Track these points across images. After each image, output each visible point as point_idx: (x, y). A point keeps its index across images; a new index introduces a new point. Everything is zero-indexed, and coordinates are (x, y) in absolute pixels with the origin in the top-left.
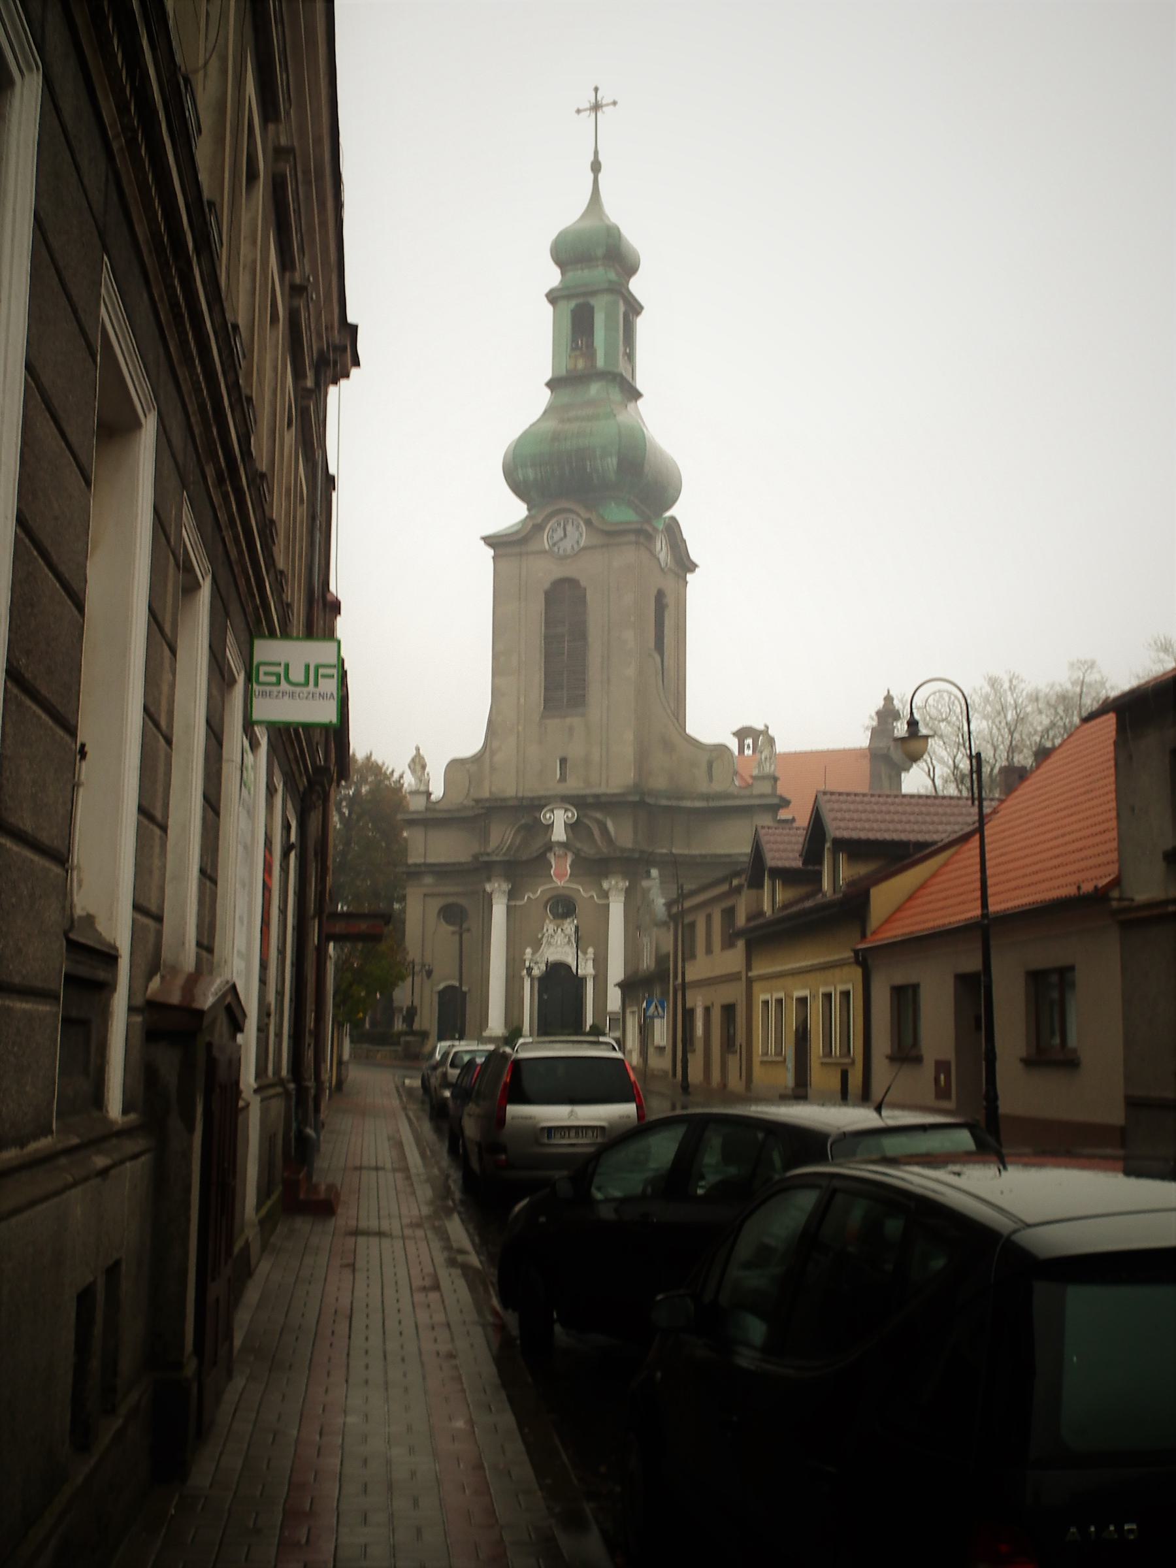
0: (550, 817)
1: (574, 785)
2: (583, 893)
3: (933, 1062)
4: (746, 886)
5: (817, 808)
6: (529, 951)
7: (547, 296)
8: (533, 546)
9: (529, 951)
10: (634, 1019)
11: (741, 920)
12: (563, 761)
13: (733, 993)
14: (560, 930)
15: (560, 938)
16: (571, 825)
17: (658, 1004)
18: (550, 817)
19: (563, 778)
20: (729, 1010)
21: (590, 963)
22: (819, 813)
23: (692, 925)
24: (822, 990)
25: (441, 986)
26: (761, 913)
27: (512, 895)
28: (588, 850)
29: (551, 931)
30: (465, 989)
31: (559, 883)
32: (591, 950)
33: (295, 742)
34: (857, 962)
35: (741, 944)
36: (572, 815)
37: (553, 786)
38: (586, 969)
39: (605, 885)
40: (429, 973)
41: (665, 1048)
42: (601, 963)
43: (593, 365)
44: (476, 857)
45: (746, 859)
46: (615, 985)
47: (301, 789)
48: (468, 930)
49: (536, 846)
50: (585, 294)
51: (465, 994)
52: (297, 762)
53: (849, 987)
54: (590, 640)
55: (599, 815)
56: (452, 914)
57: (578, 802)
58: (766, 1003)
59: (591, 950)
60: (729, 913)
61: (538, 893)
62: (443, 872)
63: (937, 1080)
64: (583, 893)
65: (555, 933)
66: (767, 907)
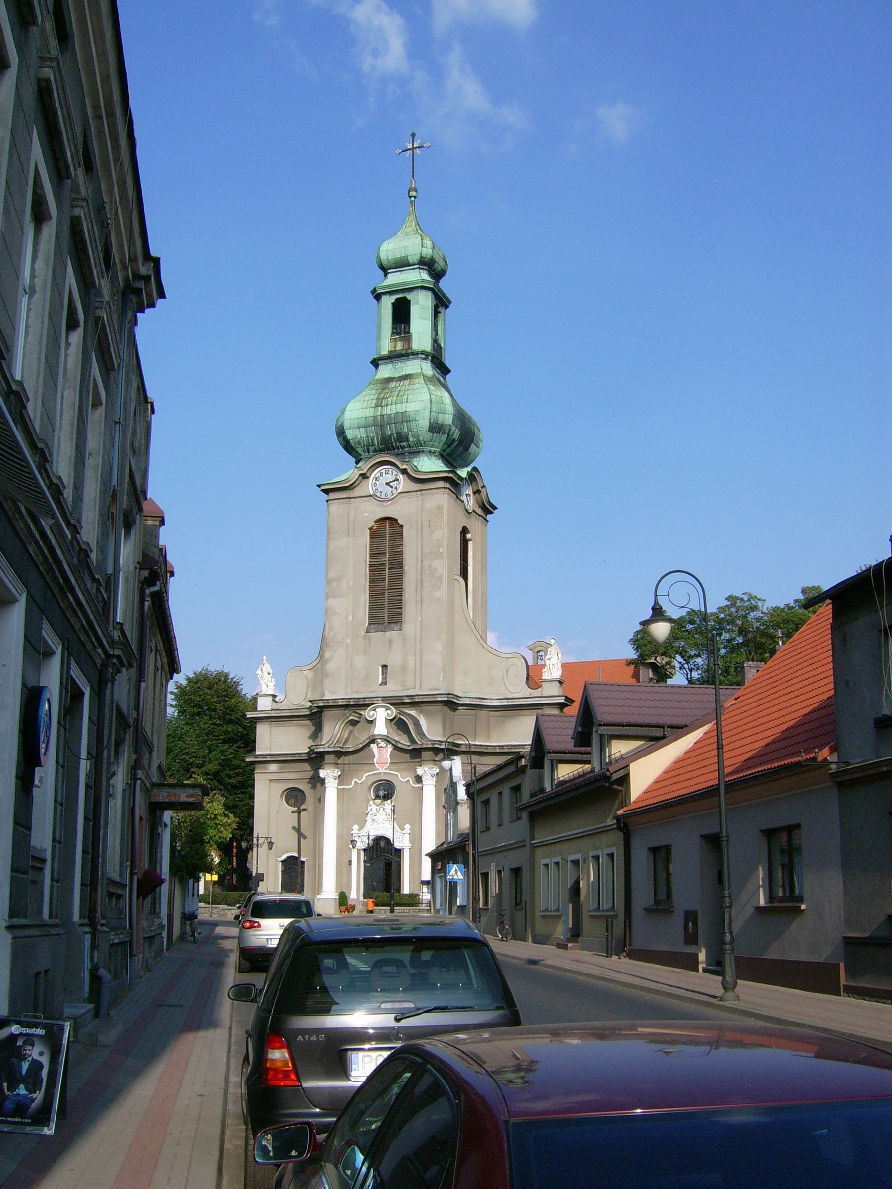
0: (373, 714)
1: (393, 689)
2: (402, 779)
3: (158, 256)
4: (529, 768)
5: (586, 696)
6: (356, 827)
7: (371, 292)
8: (357, 492)
9: (356, 827)
10: (441, 883)
11: (525, 797)
12: (384, 667)
13: (517, 859)
14: (381, 809)
15: (381, 816)
16: (391, 720)
17: (457, 869)
18: (373, 714)
19: (384, 683)
20: (517, 872)
21: (407, 837)
22: (588, 704)
23: (486, 802)
24: (592, 853)
25: (284, 857)
26: (542, 790)
27: (341, 779)
28: (404, 741)
29: (374, 811)
30: (302, 859)
31: (381, 770)
32: (408, 827)
33: (78, 610)
34: (619, 828)
35: (525, 815)
36: (393, 712)
37: (377, 690)
38: (402, 841)
39: (420, 771)
40: (271, 844)
41: (465, 906)
42: (416, 839)
43: (410, 348)
44: (311, 750)
45: (528, 749)
46: (426, 855)
47: (98, 662)
48: (304, 810)
49: (363, 738)
50: (402, 291)
51: (303, 862)
52: (86, 633)
53: (613, 850)
54: (406, 568)
55: (413, 712)
56: (294, 796)
57: (396, 702)
58: (546, 865)
59: (408, 827)
60: (517, 789)
61: (364, 778)
62: (284, 761)
63: (686, 927)
64: (402, 779)
65: (378, 812)
66: (548, 787)
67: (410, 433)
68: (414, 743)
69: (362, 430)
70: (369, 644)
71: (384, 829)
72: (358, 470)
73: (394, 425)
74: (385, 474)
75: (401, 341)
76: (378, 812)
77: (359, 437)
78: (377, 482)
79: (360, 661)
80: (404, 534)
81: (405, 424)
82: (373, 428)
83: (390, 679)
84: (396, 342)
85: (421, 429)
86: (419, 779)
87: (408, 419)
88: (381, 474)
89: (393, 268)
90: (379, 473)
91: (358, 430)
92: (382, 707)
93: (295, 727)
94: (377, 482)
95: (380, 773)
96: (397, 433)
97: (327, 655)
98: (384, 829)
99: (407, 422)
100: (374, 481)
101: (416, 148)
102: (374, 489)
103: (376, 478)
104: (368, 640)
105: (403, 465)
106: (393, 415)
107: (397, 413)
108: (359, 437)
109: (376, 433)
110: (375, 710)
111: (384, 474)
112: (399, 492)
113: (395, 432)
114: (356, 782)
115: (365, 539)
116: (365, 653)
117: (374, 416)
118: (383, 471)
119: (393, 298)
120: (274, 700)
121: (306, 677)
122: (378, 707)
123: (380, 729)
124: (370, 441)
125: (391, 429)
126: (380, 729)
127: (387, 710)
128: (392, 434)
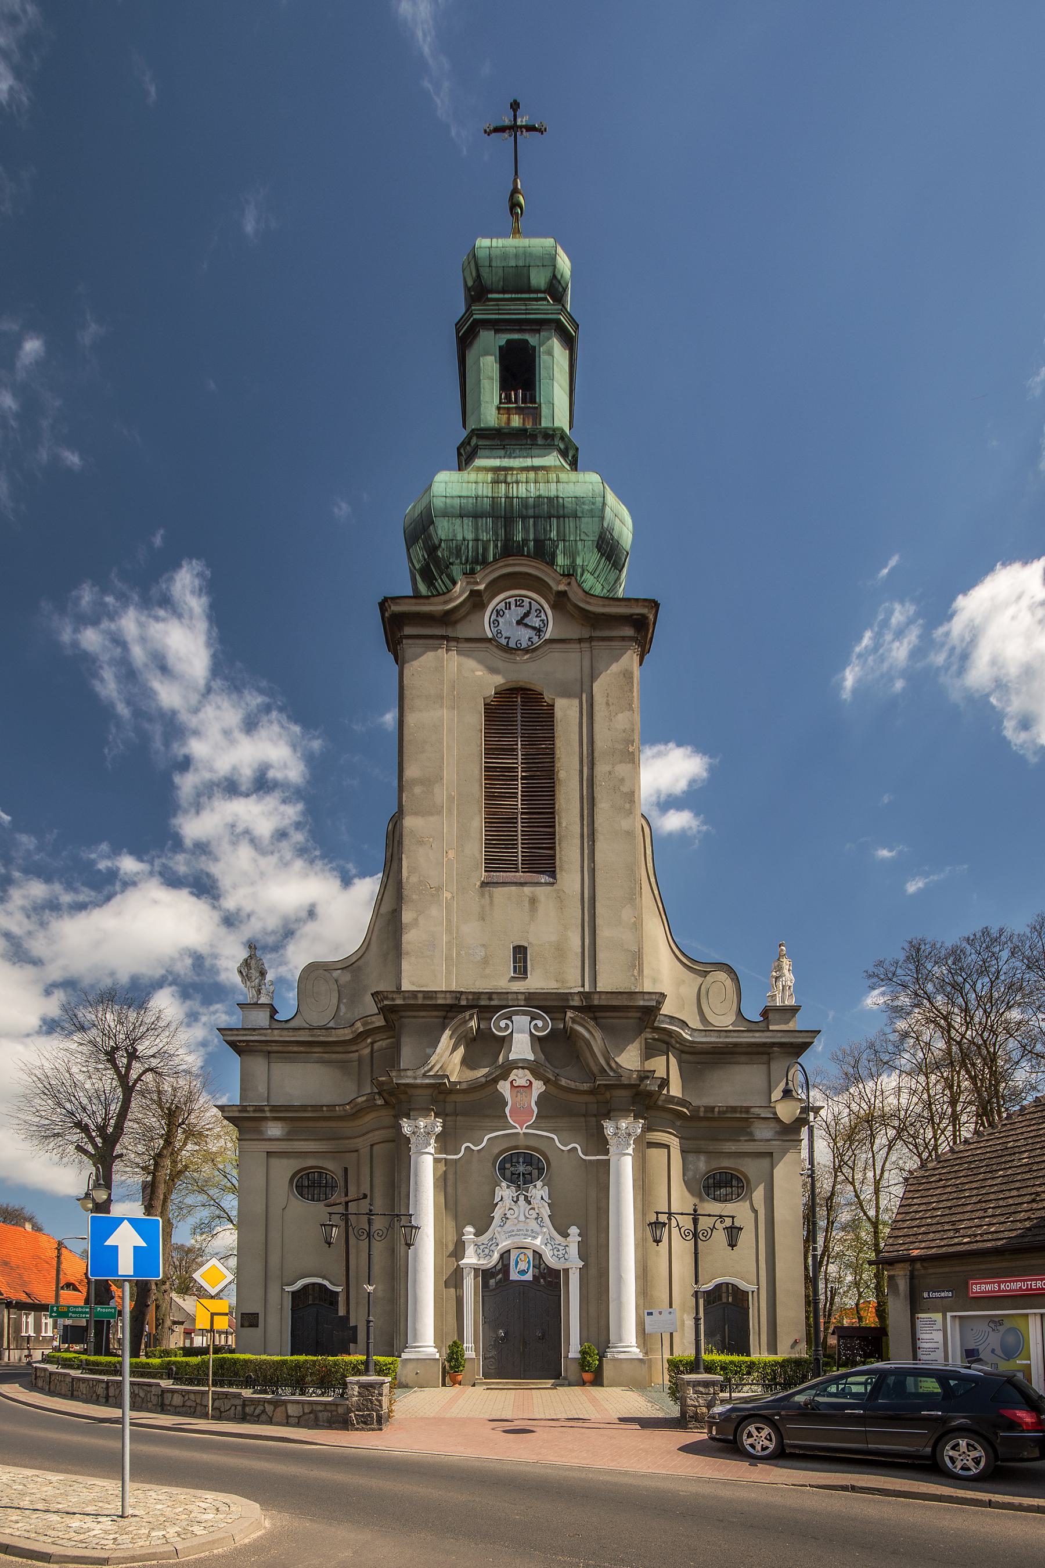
8: (464, 630)
14: (522, 1198)
27: (446, 1141)
29: (508, 1202)
32: (574, 1230)
36: (544, 1026)
59: (574, 1230)
67: (561, 545)
68: (604, 1074)
69: (468, 522)
70: (491, 903)
71: (529, 1233)
72: (468, 583)
73: (531, 521)
74: (516, 606)
75: (519, 414)
76: (516, 1202)
77: (460, 537)
78: (500, 620)
79: (471, 930)
80: (556, 715)
81: (554, 521)
82: (490, 520)
83: (532, 969)
84: (509, 415)
85: (583, 537)
86: (601, 1144)
87: (561, 512)
88: (508, 606)
89: (499, 293)
90: (503, 604)
91: (458, 521)
92: (525, 1013)
93: (316, 1065)
94: (500, 620)
95: (518, 1133)
96: (535, 541)
97: (407, 916)
98: (529, 1233)
99: (558, 517)
100: (494, 617)
101: (521, 127)
102: (494, 630)
103: (498, 612)
104: (487, 896)
105: (559, 583)
106: (531, 500)
107: (539, 497)
108: (460, 537)
109: (496, 533)
110: (510, 1018)
111: (513, 607)
112: (547, 636)
113: (532, 537)
114: (467, 1148)
115: (476, 719)
116: (482, 918)
117: (492, 497)
118: (512, 600)
119: (503, 339)
120: (272, 1017)
121: (336, 981)
122: (516, 1013)
123: (521, 1048)
124: (481, 551)
125: (526, 529)
126: (521, 1048)
127: (533, 1019)
128: (525, 541)
